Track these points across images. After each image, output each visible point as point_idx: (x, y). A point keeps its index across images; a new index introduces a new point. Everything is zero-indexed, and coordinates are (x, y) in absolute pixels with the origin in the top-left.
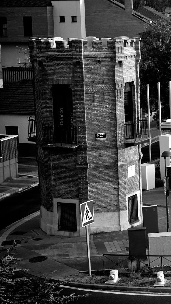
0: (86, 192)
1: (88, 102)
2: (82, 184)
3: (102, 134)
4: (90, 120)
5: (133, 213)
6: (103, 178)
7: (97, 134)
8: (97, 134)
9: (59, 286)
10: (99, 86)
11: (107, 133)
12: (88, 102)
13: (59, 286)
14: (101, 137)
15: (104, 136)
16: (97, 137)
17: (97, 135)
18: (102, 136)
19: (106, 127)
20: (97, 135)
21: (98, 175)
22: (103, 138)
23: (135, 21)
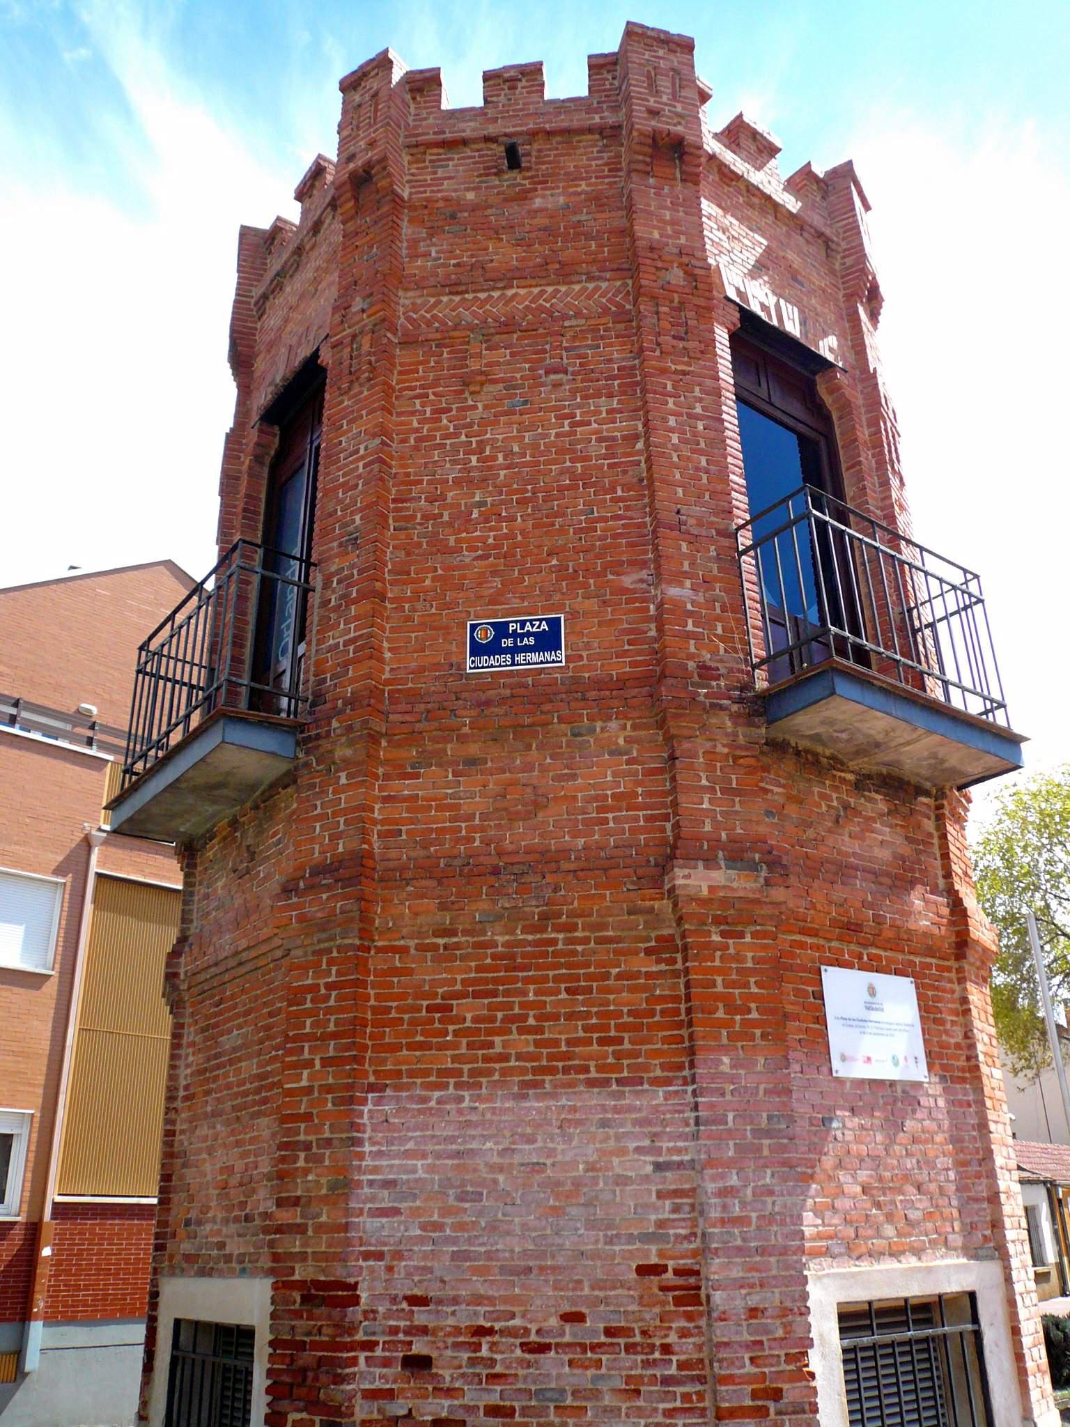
0: (333, 1187)
1: (416, 397)
2: (308, 1090)
3: (523, 624)
4: (426, 518)
5: (906, 591)
6: (526, 1044)
7: (474, 627)
8: (474, 627)
9: (394, 82)
10: (510, 293)
11: (573, 616)
12: (416, 397)
13: (394, 82)
14: (514, 651)
15: (548, 641)
16: (477, 650)
17: (478, 635)
18: (522, 636)
19: (562, 568)
20: (478, 635)
21: (469, 1010)
22: (535, 657)
23: (980, 770)
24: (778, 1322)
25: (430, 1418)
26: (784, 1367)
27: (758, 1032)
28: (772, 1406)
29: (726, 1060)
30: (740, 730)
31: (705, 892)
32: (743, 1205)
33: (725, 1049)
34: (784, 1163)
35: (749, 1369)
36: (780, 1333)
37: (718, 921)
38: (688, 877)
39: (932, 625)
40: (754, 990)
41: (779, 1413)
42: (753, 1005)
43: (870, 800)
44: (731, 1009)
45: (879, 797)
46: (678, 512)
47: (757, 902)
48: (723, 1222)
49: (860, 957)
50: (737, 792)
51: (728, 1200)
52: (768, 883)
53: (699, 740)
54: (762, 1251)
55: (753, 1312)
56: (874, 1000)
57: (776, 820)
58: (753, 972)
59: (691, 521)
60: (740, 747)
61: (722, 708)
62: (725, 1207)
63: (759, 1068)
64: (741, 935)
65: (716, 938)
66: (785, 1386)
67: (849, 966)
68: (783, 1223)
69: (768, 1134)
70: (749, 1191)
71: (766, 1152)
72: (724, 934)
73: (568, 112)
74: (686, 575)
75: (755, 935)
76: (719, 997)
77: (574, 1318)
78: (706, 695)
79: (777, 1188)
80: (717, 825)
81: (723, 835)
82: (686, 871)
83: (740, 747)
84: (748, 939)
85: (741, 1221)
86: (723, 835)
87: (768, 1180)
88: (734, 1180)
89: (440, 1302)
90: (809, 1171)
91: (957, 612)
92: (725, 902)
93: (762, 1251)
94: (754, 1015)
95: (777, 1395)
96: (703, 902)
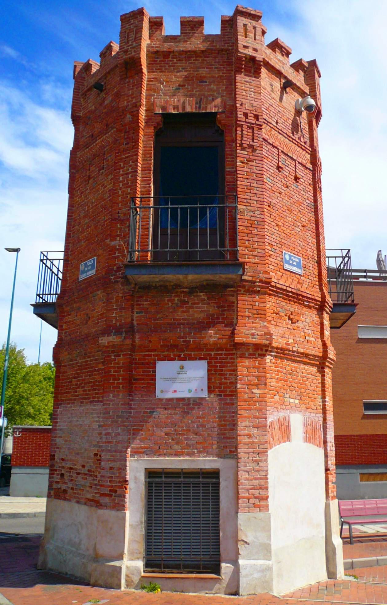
24: (118, 472)
25: (334, 504)
26: (118, 484)
27: (121, 386)
28: (114, 494)
29: (111, 395)
30: (125, 287)
31: (106, 344)
32: (112, 438)
33: (111, 392)
34: (124, 426)
35: (109, 484)
36: (118, 475)
37: (113, 352)
38: (102, 340)
39: (56, 294)
40: (122, 373)
41: (115, 496)
42: (121, 378)
43: (197, 296)
44: (114, 380)
45: (202, 294)
46: (118, 213)
47: (122, 345)
48: (106, 442)
49: (180, 355)
50: (124, 309)
51: (108, 436)
52: (125, 338)
53: (114, 294)
54: (115, 451)
55: (111, 468)
56: (183, 370)
57: (144, 314)
58: (122, 367)
59: (122, 215)
60: (126, 293)
61: (117, 282)
62: (107, 438)
63: (120, 397)
64: (119, 356)
65: (113, 357)
66: (118, 489)
67: (173, 359)
68: (121, 443)
69: (120, 417)
70: (113, 434)
71: (119, 422)
72: (115, 356)
73: (136, 33)
74: (117, 236)
75: (123, 355)
76: (111, 376)
77: (83, 466)
78: (114, 279)
79: (121, 433)
80: (116, 321)
81: (118, 324)
82: (102, 338)
83: (126, 293)
84: (122, 357)
85: (109, 442)
86: (118, 324)
87: (119, 431)
88: (110, 431)
89: (68, 460)
90: (141, 428)
91: (48, 294)
92: (113, 346)
93: (115, 451)
94: (121, 381)
95: (116, 491)
96: (107, 347)
